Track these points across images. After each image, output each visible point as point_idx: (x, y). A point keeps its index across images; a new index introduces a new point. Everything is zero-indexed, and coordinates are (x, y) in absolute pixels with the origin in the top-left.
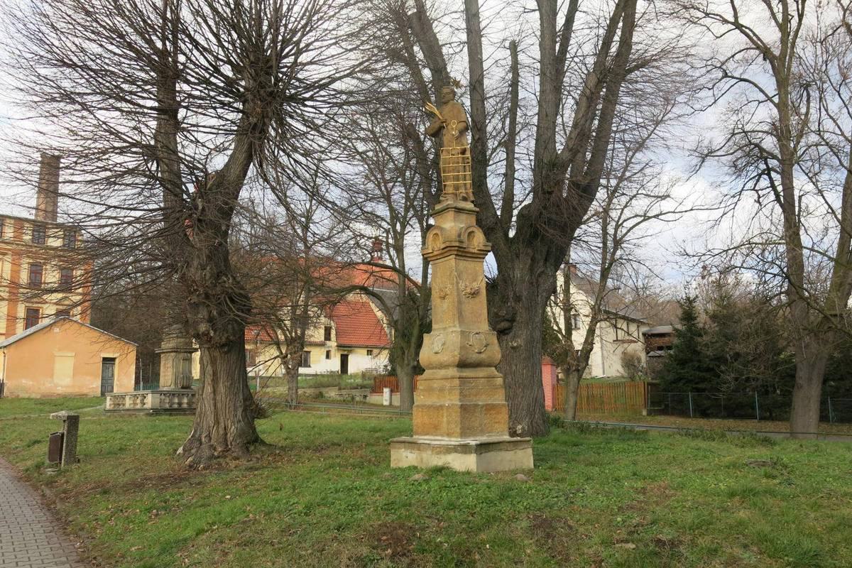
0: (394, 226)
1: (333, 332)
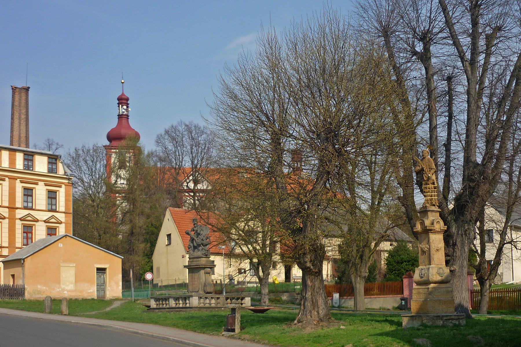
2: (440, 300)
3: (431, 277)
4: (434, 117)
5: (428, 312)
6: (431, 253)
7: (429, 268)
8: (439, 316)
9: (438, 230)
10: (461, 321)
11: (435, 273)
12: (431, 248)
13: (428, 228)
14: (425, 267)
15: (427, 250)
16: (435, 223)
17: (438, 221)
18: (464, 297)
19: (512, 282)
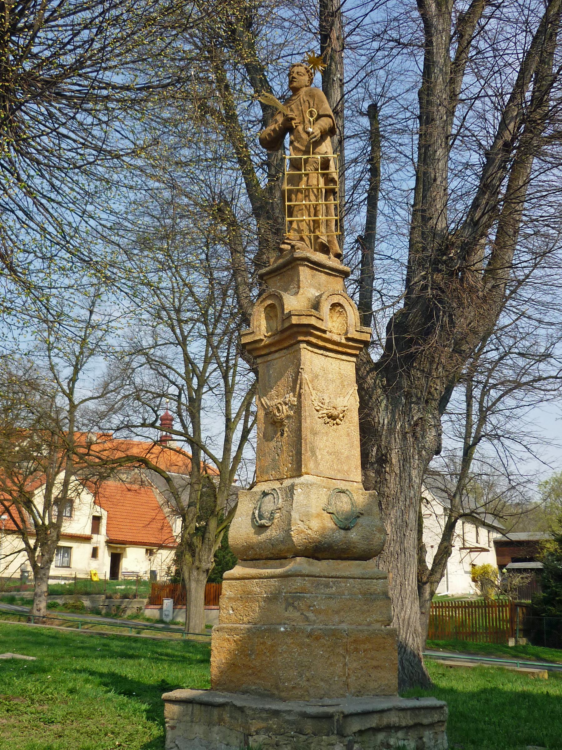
0: (189, 380)
1: (104, 522)
2: (334, 633)
3: (302, 526)
4: (336, 86)
5: (277, 688)
6: (306, 424)
7: (292, 488)
8: (328, 717)
9: (336, 338)
10: (427, 735)
11: (319, 510)
12: (306, 403)
13: (294, 322)
14: (276, 485)
15: (288, 417)
16: (325, 307)
17: (339, 305)
18: (409, 619)
19: (446, 593)
